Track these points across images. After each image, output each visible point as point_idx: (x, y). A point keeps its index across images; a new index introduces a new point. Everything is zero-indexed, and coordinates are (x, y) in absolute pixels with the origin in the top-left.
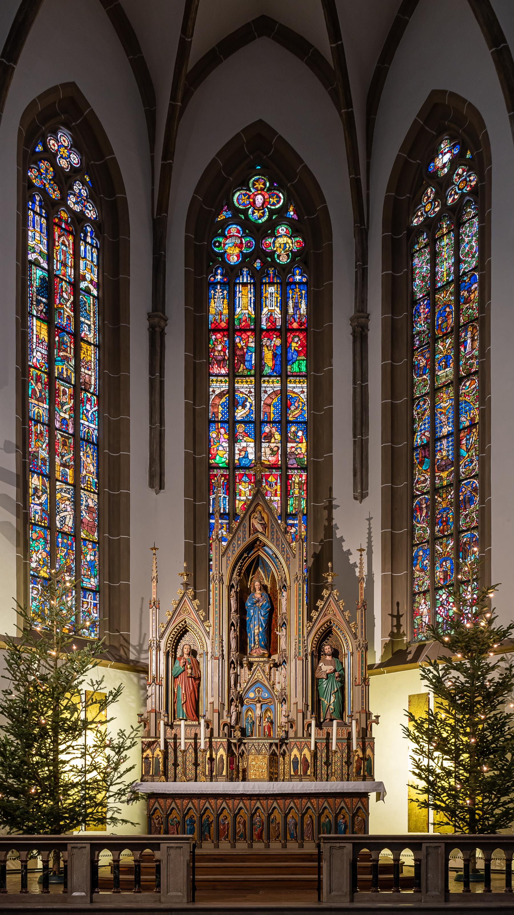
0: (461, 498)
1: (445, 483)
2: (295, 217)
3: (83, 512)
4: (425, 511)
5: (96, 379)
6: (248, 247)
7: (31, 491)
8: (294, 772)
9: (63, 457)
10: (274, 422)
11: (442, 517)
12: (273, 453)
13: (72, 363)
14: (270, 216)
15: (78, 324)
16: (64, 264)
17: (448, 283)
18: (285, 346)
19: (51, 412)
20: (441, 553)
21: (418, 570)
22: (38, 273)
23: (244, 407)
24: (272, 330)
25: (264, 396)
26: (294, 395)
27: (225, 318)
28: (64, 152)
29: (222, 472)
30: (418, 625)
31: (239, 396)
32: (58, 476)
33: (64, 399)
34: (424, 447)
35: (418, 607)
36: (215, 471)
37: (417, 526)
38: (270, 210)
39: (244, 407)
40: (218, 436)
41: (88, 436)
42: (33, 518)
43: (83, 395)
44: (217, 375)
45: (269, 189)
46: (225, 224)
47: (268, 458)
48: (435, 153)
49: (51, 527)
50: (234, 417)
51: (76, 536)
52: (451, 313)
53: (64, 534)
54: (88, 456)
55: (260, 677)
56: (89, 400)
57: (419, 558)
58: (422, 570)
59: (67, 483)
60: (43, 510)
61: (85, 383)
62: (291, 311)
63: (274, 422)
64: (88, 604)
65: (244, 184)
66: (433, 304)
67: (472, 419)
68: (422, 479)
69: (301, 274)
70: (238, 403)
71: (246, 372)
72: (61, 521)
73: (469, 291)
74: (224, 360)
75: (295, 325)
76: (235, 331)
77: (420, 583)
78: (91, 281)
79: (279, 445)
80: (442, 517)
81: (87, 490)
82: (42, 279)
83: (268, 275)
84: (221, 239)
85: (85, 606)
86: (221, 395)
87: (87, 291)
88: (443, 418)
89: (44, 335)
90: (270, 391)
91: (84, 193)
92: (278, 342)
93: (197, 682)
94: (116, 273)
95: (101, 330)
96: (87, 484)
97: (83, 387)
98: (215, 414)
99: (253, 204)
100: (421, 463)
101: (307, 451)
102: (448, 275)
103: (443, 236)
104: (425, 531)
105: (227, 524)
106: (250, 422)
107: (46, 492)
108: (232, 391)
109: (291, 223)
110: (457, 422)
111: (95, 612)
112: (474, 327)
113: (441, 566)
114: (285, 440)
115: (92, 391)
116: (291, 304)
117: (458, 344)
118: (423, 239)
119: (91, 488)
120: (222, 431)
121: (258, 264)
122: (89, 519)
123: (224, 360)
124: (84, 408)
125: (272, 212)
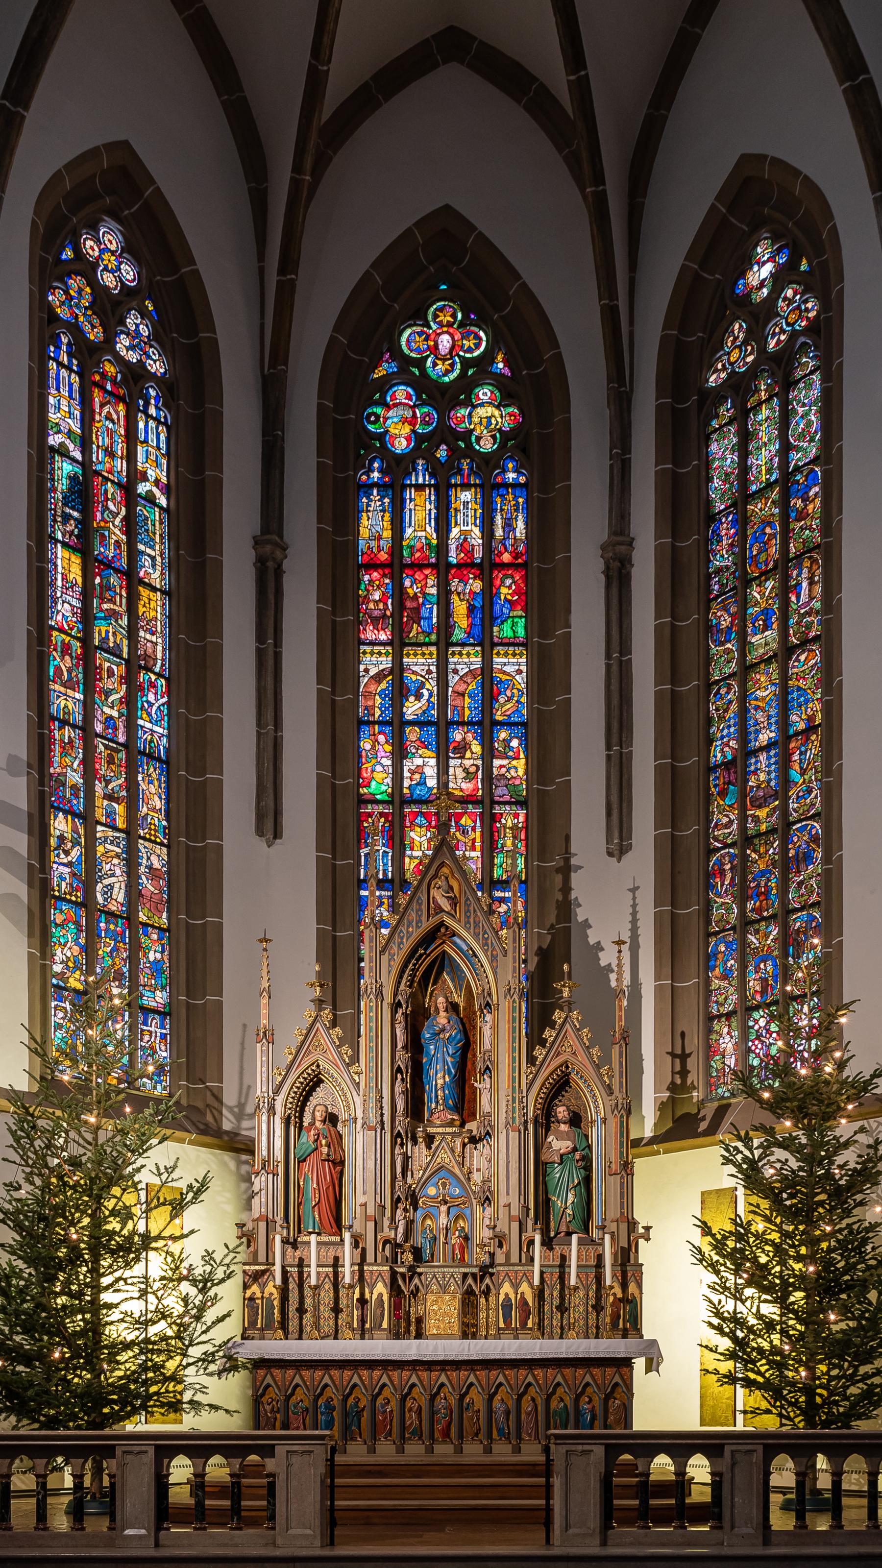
0: (792, 853)
1: (763, 827)
2: (507, 372)
3: (143, 877)
4: (729, 876)
5: (164, 650)
6: (425, 423)
7: (53, 842)
8: (504, 1322)
9: (108, 782)
10: (470, 723)
11: (758, 886)
12: (469, 776)
13: (124, 622)
14: (464, 371)
15: (134, 555)
16: (110, 453)
17: (769, 485)
18: (490, 593)
19: (88, 707)
20: (757, 948)
21: (716, 978)
22: (65, 469)
23: (419, 697)
24: (466, 566)
25: (453, 679)
26: (504, 677)
27: (386, 544)
28: (110, 260)
29: (380, 808)
30: (717, 1070)
31: (410, 678)
32: (100, 815)
33: (109, 684)
34: (728, 765)
35: (717, 1041)
36: (369, 806)
37: (716, 902)
38: (464, 360)
39: (419, 697)
40: (373, 747)
41: (150, 747)
42: (56, 888)
43: (143, 677)
44: (372, 643)
45: (462, 325)
46: (386, 384)
47: (460, 784)
48: (747, 262)
49: (87, 903)
50: (402, 714)
51: (130, 919)
52: (773, 536)
53: (110, 914)
54: (151, 782)
55: (447, 1160)
56: (153, 685)
57: (720, 956)
58: (724, 977)
59: (115, 828)
60: (73, 875)
61: (146, 656)
62: (499, 533)
63: (470, 723)
64: (151, 1036)
65: (418, 316)
66: (742, 521)
67: (811, 719)
68: (725, 820)
69: (516, 470)
70: (409, 690)
71: (421, 638)
72: (105, 893)
73: (806, 499)
74: (384, 616)
75: (506, 557)
76: (404, 567)
77: (721, 999)
78: (157, 482)
79: (479, 762)
80: (758, 886)
81: (150, 840)
82: (73, 478)
83: (460, 471)
84: (379, 410)
85: (146, 1038)
86: (379, 677)
87: (150, 499)
88: (760, 716)
89: (76, 573)
90: (463, 670)
91: (144, 331)
92: (476, 586)
93: (338, 1168)
94: (198, 467)
95: (173, 566)
96: (150, 829)
97: (143, 663)
98: (370, 709)
99: (435, 349)
100: (723, 794)
101: (526, 772)
102: (769, 471)
103: (760, 404)
104: (729, 909)
105: (389, 897)
106: (429, 723)
107: (79, 844)
108: (398, 670)
109: (499, 381)
110: (784, 723)
111: (163, 1048)
112: (814, 561)
113: (757, 970)
114: (489, 754)
115: (157, 670)
116: (499, 520)
117: (786, 590)
118: (726, 410)
119: (156, 836)
120: (381, 738)
121: (442, 453)
122: (152, 889)
123: (384, 616)
124: (144, 699)
125: (466, 364)
